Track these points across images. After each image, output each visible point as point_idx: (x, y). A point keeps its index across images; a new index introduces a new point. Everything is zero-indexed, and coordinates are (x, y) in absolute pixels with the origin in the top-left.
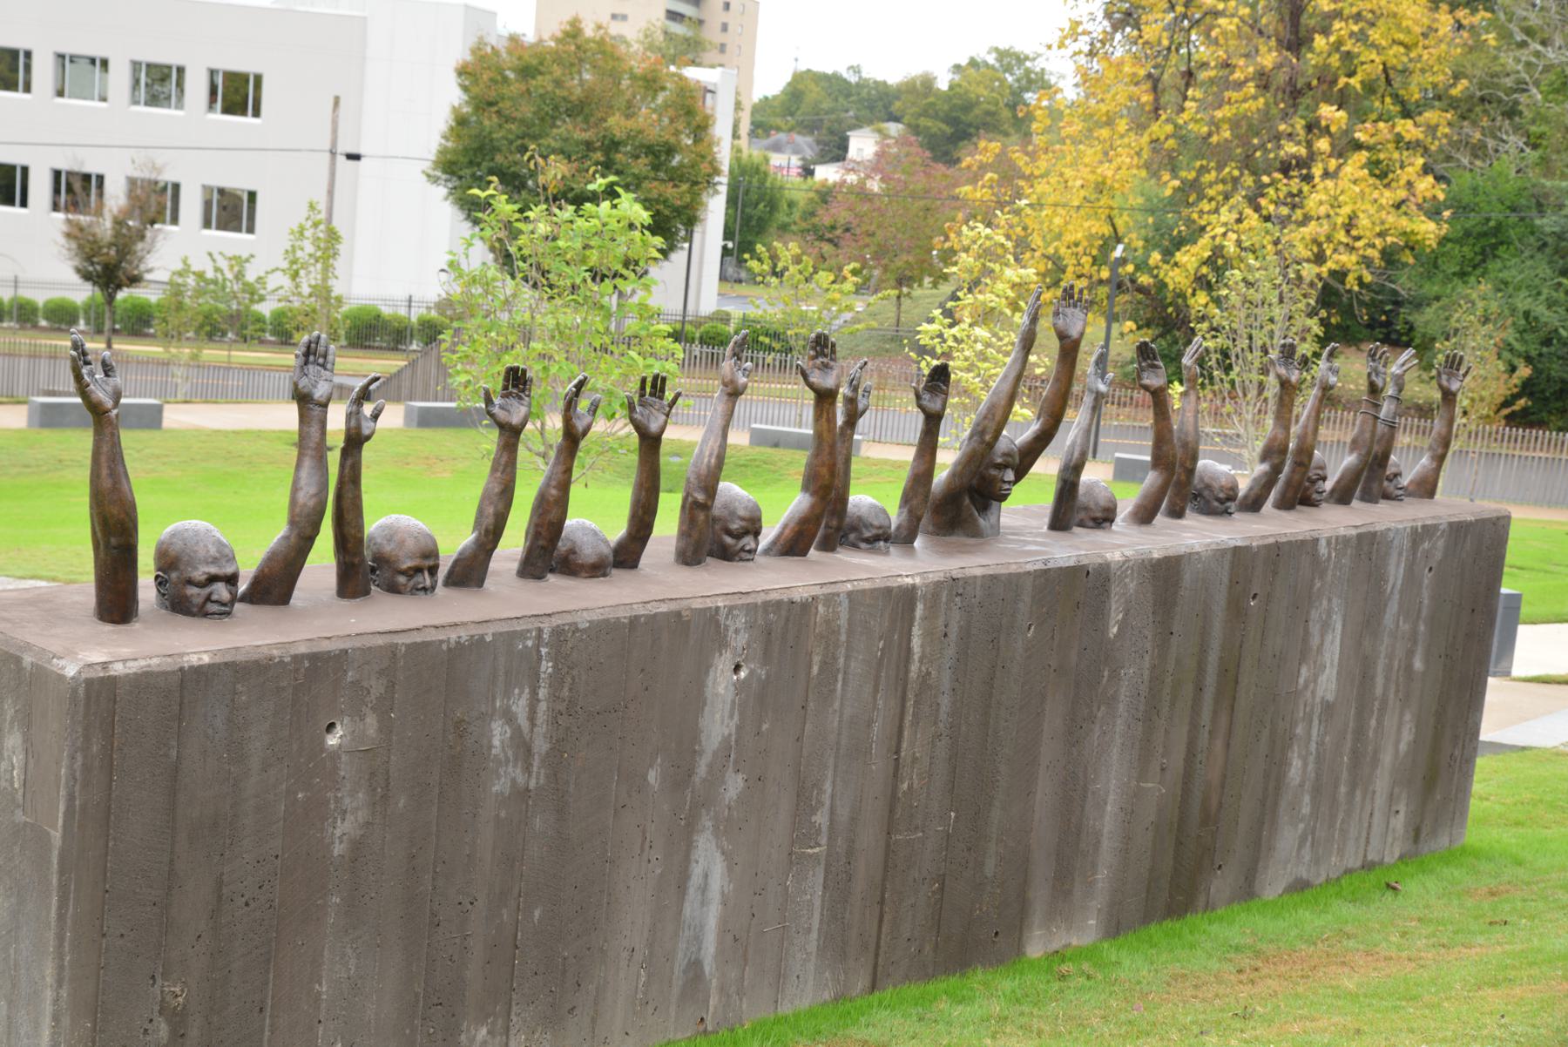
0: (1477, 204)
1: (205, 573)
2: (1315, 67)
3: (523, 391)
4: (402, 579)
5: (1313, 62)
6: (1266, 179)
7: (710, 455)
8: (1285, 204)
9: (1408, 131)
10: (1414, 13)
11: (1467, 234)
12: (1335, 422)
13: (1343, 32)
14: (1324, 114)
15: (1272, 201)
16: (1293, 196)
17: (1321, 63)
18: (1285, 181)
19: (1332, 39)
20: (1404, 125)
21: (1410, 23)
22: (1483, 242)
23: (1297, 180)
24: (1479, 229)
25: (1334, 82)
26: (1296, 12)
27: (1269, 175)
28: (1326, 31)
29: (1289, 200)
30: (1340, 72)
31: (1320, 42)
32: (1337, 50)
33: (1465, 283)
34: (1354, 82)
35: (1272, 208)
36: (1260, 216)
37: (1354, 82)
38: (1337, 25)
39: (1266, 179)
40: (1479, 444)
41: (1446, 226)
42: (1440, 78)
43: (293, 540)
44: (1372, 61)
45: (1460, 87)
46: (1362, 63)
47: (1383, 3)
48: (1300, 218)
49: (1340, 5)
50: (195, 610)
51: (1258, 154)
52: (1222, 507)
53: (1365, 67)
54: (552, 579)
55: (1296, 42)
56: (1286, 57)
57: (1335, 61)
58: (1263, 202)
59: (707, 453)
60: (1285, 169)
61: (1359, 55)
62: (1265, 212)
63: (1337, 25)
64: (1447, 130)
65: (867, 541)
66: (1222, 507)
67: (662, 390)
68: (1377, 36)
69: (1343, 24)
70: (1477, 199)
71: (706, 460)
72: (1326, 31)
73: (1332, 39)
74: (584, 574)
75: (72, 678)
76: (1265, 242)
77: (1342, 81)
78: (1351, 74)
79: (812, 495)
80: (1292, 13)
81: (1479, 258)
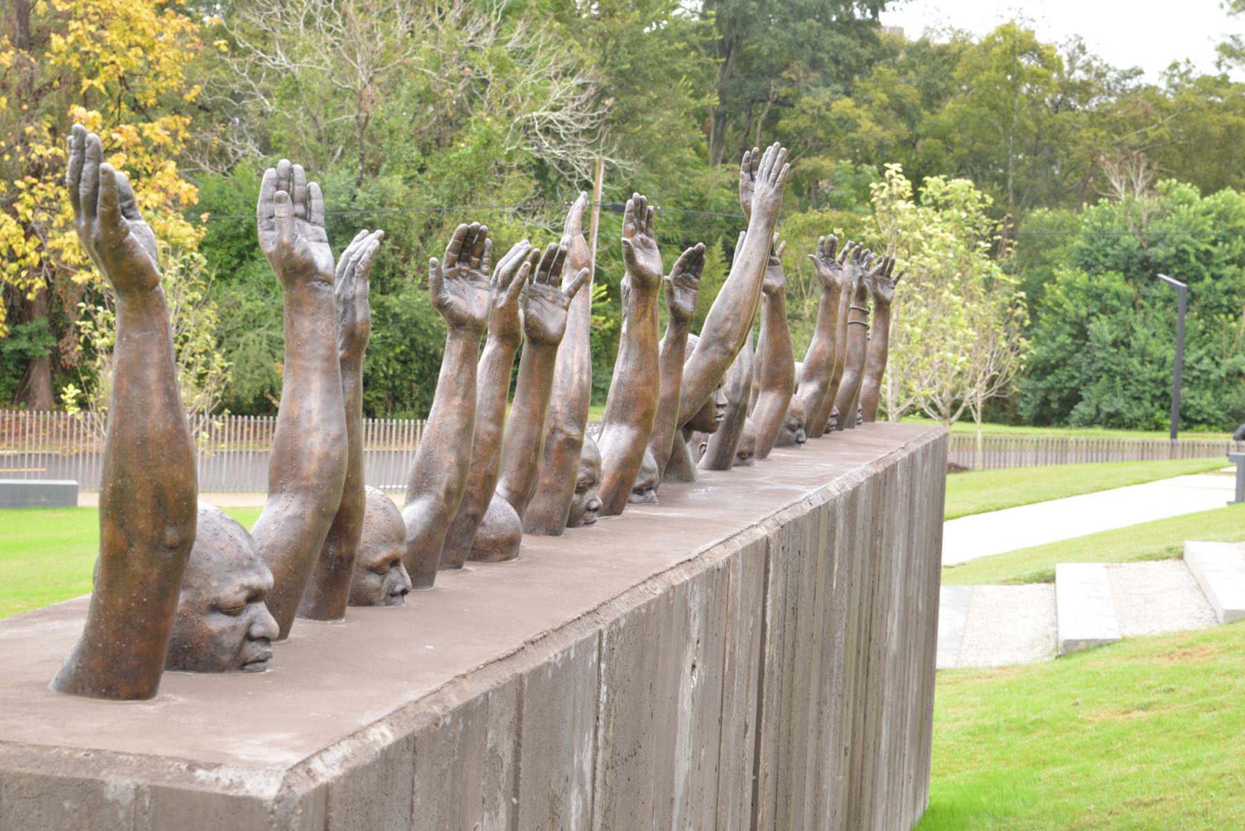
0: (226, 207)
1: (243, 587)
2: (54, 66)
3: (478, 267)
4: (373, 580)
5: (52, 62)
6: (19, 184)
7: (581, 370)
8: (42, 209)
9: (157, 134)
10: (145, 14)
11: (221, 238)
12: (71, 436)
13: (80, 32)
14: (77, 114)
15: (28, 207)
16: (50, 200)
17: (60, 63)
18: (41, 185)
19: (70, 39)
20: (152, 129)
21: (145, 25)
22: (238, 244)
23: (52, 184)
24: (231, 231)
25: (78, 83)
26: (24, 11)
27: (22, 179)
28: (63, 31)
29: (47, 205)
30: (82, 73)
31: (57, 41)
32: (76, 50)
33: (229, 285)
34: (97, 83)
35: (29, 213)
36: (18, 222)
37: (97, 83)
38: (73, 25)
39: (19, 184)
40: (245, 445)
41: (204, 229)
42: (174, 83)
43: (309, 518)
44: (113, 63)
45: (193, 93)
46: (104, 64)
47: (116, 4)
48: (62, 224)
49: (73, 4)
50: (226, 658)
51: (7, 157)
52: (793, 435)
53: (106, 68)
54: (469, 567)
55: (33, 41)
56: (22, 56)
57: (74, 62)
58: (19, 207)
59: (576, 368)
60: (37, 172)
61: (97, 56)
62: (22, 218)
63: (73, 25)
64: (187, 135)
65: (640, 491)
66: (793, 435)
67: (557, 271)
68: (114, 37)
69: (79, 23)
70: (225, 203)
71: (576, 377)
72: (63, 31)
73: (70, 39)
74: (499, 556)
75: (278, 800)
76: (28, 250)
77: (86, 83)
78: (93, 75)
79: (632, 427)
80: (19, 11)
81: (236, 261)
